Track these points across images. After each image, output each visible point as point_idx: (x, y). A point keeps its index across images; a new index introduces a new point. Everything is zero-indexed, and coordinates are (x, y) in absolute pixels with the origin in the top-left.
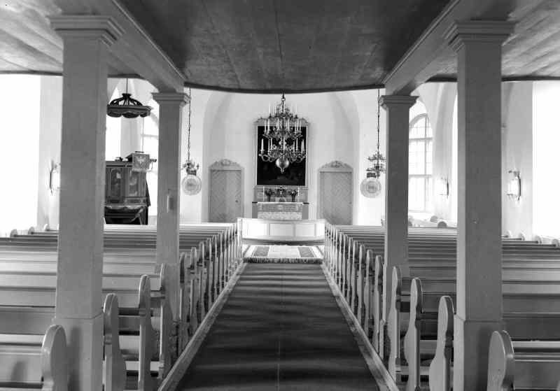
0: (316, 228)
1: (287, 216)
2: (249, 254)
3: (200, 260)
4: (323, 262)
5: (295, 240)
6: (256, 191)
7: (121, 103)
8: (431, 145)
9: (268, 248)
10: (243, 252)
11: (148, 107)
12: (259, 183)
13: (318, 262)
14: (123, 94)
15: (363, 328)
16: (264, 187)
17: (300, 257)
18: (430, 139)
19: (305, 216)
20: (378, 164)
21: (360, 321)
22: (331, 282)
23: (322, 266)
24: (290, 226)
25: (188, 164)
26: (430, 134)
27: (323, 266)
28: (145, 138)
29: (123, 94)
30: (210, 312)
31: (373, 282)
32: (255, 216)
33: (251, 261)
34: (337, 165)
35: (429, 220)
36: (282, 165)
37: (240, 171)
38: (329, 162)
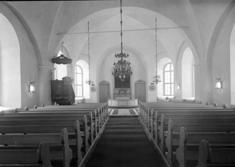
0: (135, 102)
1: (125, 98)
2: (111, 114)
3: (105, 107)
4: (139, 117)
5: (127, 106)
6: (114, 90)
7: (61, 58)
8: (173, 73)
9: (118, 110)
10: (109, 113)
11: (70, 59)
12: (115, 88)
13: (136, 116)
14: (61, 55)
15: (159, 147)
16: (117, 89)
17: (130, 115)
18: (172, 71)
19: (131, 98)
20: (157, 79)
21: (157, 142)
22: (146, 130)
23: (138, 118)
24: (126, 102)
25: (89, 82)
26: (172, 69)
27: (140, 118)
28: (77, 74)
29: (61, 55)
30: (92, 145)
31: (145, 111)
32: (114, 99)
33: (111, 117)
34: (140, 81)
35: (165, 99)
36: (122, 78)
37: (109, 84)
38: (138, 80)
